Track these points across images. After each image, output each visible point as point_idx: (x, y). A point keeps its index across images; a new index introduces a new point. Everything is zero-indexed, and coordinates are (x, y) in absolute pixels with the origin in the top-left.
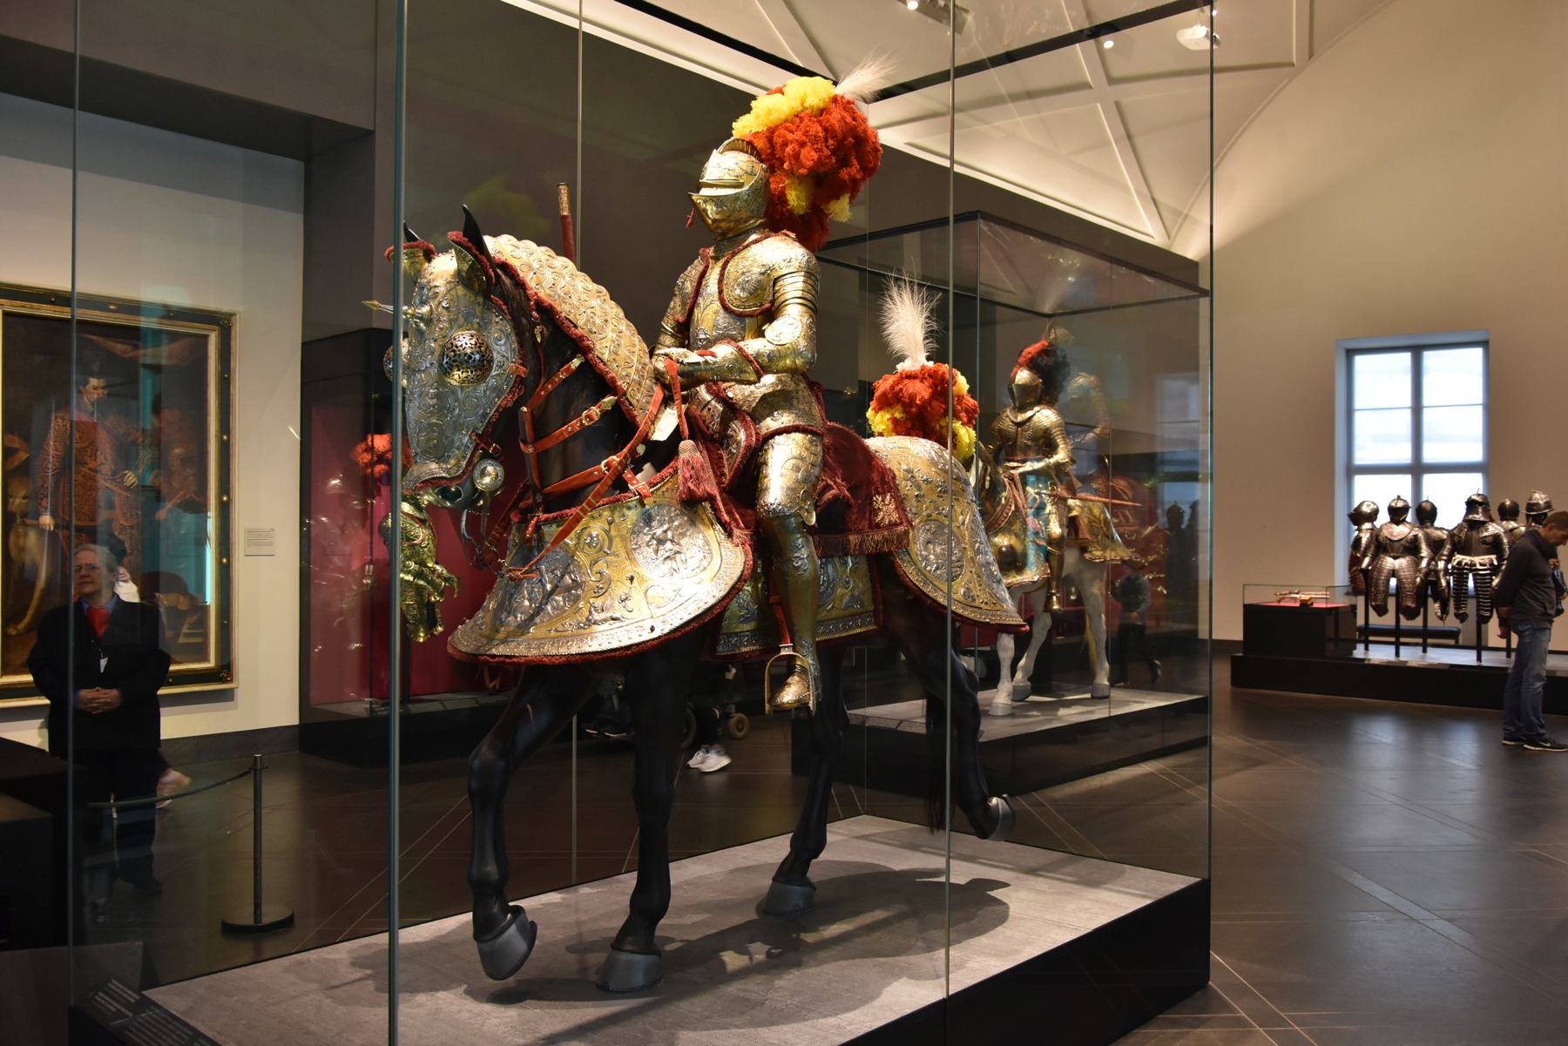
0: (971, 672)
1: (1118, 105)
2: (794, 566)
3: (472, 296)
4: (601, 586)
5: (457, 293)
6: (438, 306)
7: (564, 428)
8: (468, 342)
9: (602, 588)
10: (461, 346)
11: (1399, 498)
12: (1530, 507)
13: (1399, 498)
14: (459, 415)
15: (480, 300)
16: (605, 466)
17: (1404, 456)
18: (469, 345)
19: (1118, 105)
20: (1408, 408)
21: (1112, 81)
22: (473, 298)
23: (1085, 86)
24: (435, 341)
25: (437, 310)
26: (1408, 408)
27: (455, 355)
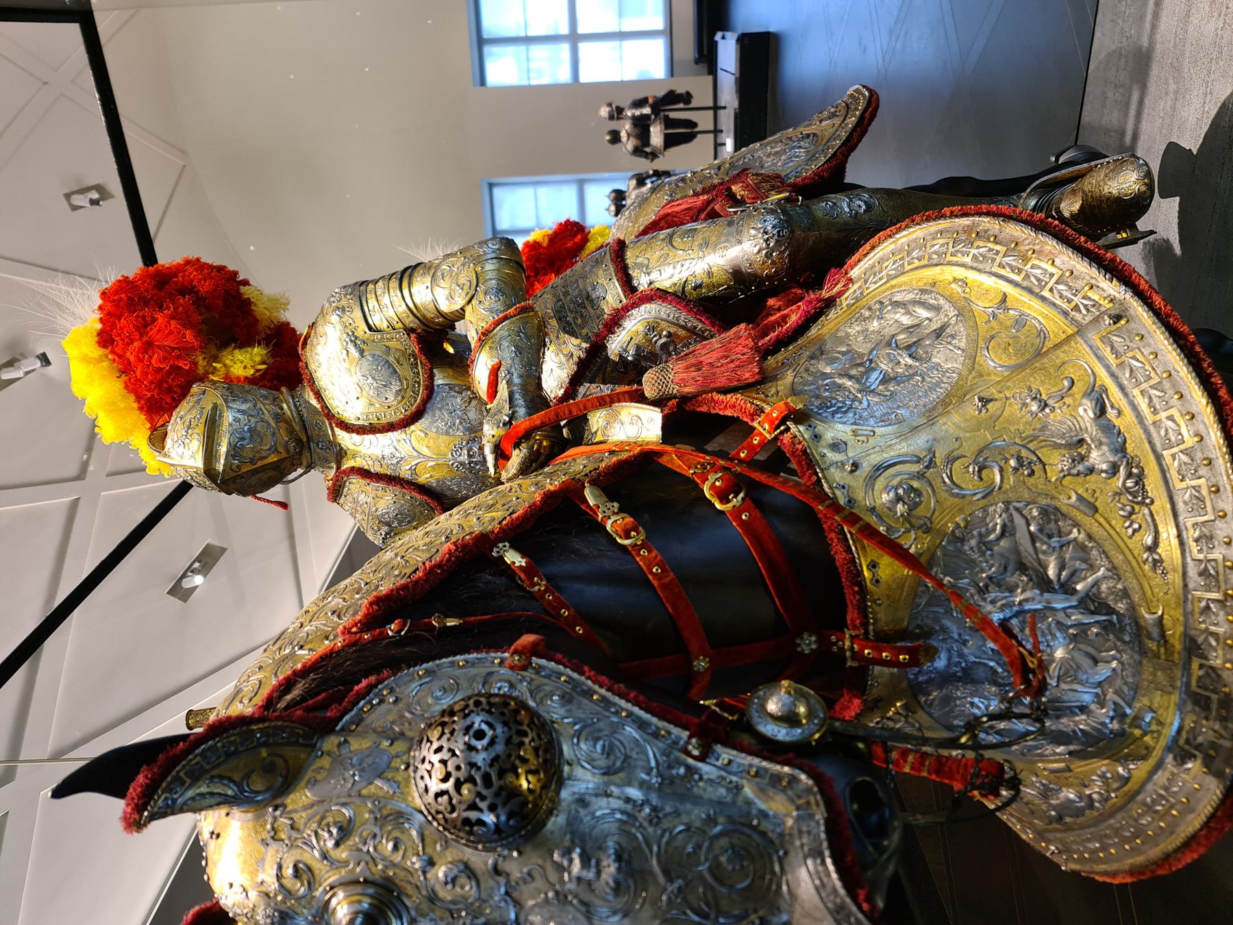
0: (929, 639)
1: (110, 474)
2: (865, 211)
3: (318, 763)
4: (1012, 463)
5: (305, 808)
6: (334, 864)
7: (655, 583)
8: (435, 745)
9: (1019, 459)
10: (444, 762)
11: (608, 210)
12: (611, 117)
13: (608, 210)
14: (642, 785)
15: (331, 743)
16: (729, 501)
17: (583, 47)
18: (444, 742)
19: (110, 474)
20: (527, 50)
21: (81, 475)
22: (326, 762)
23: (74, 505)
24: (431, 863)
25: (346, 863)
26: (527, 50)
27: (470, 780)
